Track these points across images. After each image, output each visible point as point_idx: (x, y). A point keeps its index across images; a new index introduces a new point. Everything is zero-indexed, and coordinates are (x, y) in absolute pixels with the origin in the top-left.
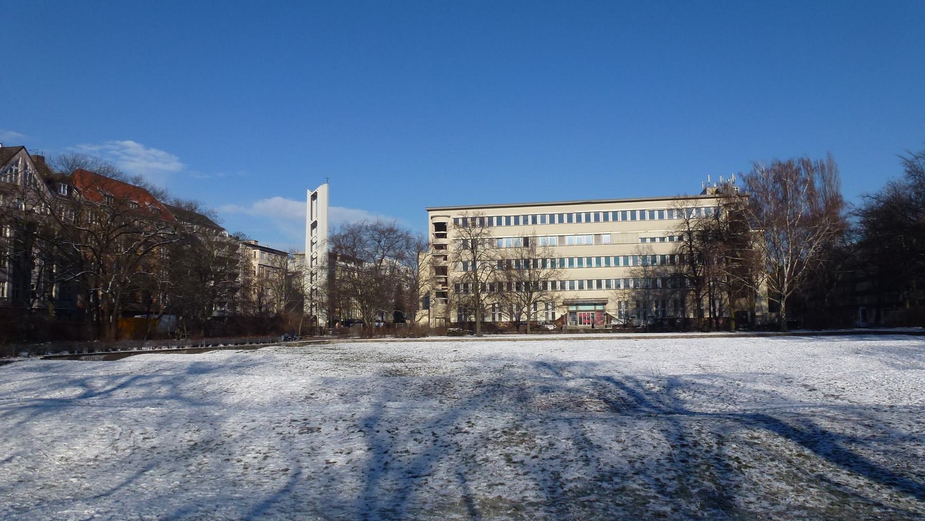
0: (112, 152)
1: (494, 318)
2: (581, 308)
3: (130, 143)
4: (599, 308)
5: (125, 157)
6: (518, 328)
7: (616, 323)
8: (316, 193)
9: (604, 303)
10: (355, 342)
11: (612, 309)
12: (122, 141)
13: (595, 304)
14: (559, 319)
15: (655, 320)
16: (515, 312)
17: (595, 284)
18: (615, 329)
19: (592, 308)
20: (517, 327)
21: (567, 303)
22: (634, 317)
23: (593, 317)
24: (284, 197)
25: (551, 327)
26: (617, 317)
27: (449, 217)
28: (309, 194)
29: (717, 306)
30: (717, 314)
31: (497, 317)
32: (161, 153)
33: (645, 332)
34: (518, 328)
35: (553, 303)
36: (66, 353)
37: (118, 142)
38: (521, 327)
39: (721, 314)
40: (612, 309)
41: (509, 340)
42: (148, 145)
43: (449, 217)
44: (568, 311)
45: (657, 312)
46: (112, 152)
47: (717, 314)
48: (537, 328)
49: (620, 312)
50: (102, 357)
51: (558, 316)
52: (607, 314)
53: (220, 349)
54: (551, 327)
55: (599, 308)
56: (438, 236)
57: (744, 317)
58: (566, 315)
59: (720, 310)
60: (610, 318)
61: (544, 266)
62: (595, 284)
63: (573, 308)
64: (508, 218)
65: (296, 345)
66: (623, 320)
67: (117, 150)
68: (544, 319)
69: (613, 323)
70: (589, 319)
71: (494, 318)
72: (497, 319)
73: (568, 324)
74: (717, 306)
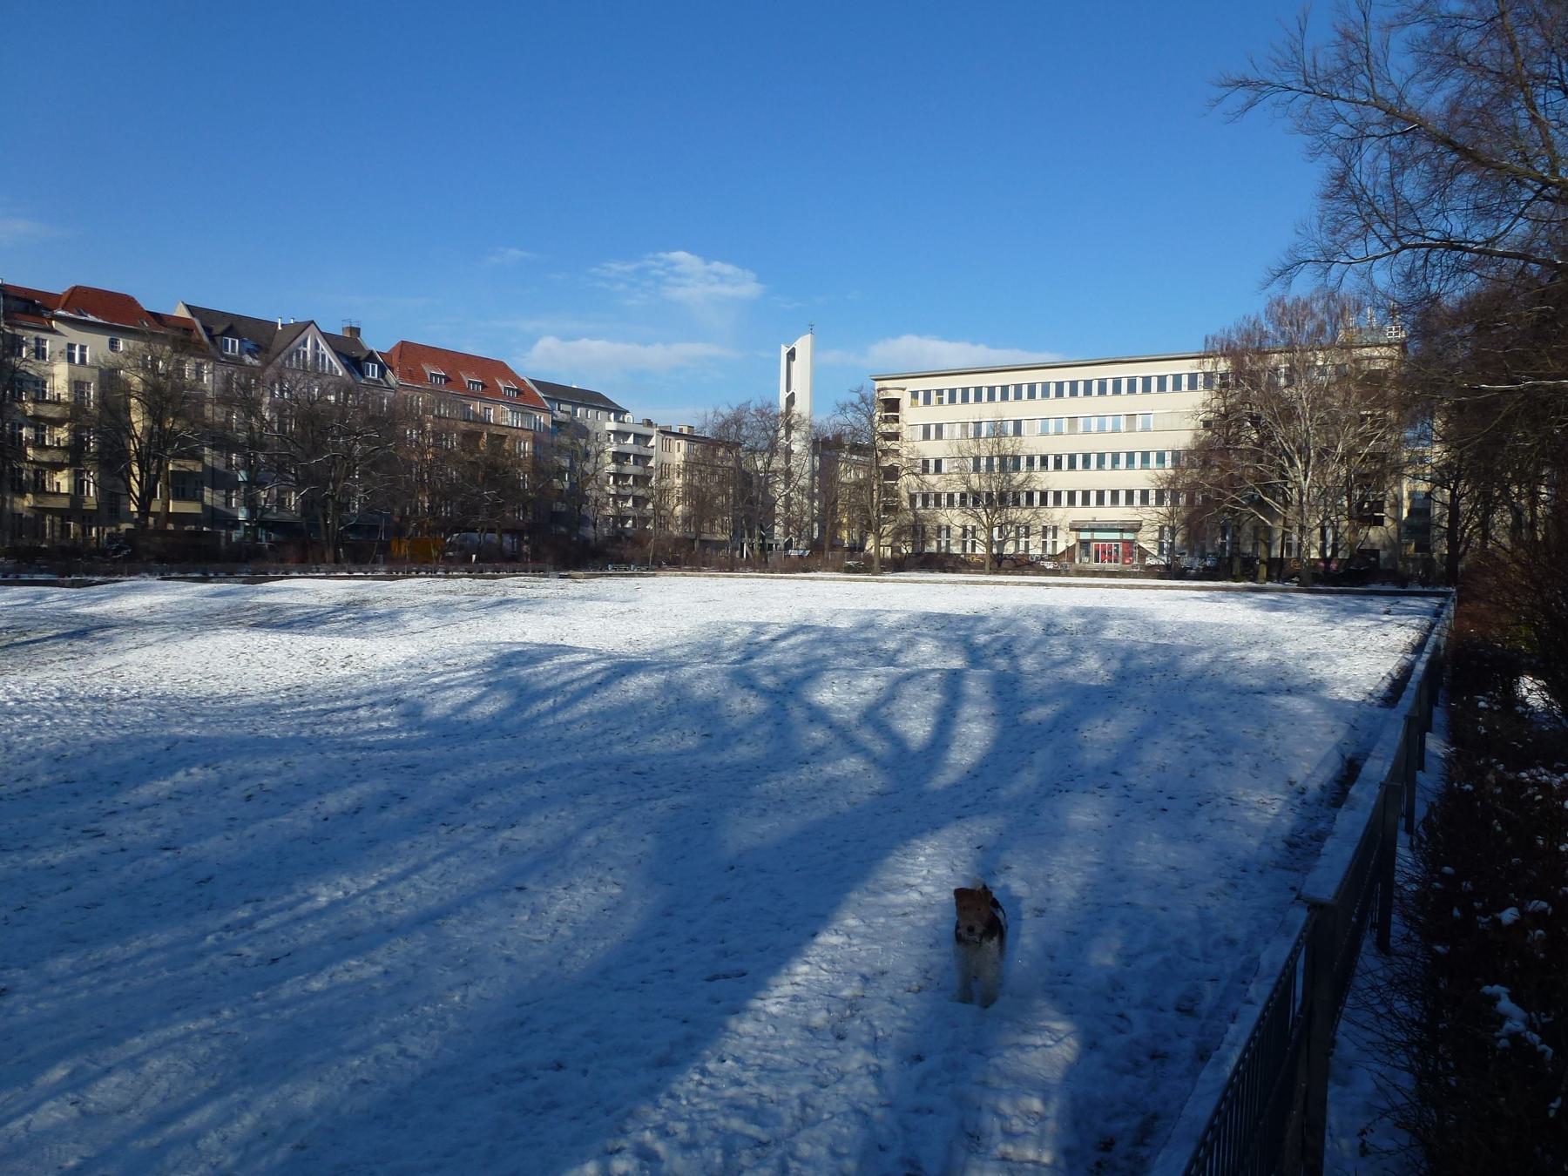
0: (653, 272)
1: (964, 548)
2: (1098, 536)
3: (680, 255)
4: (1127, 536)
5: (672, 279)
6: (999, 565)
7: (1153, 562)
8: (794, 349)
9: (1135, 528)
10: (685, 575)
11: (1147, 540)
12: (667, 251)
13: (1122, 531)
14: (1063, 553)
15: (1220, 559)
16: (997, 539)
17: (1122, 496)
18: (1151, 572)
19: (1116, 536)
20: (1000, 564)
21: (1075, 528)
22: (1184, 554)
23: (1117, 551)
24: (920, 334)
25: (1049, 565)
26: (1156, 553)
27: (904, 389)
28: (784, 351)
29: (1330, 538)
30: (1329, 553)
31: (1022, 546)
32: (728, 269)
33: (1161, 577)
34: (999, 565)
35: (1027, 528)
36: (424, 573)
37: (662, 255)
38: (1005, 564)
39: (1335, 553)
40: (1147, 540)
41: (929, 582)
42: (707, 254)
43: (904, 389)
44: (1078, 540)
45: (1223, 546)
46: (653, 272)
47: (1329, 553)
48: (1022, 565)
49: (1161, 545)
50: (241, 580)
51: (1061, 548)
52: (1139, 547)
53: (439, 577)
54: (1049, 565)
55: (1127, 536)
56: (886, 420)
57: (1373, 559)
58: (1074, 545)
59: (1334, 547)
60: (1144, 554)
61: (1017, 468)
62: (1122, 496)
63: (1085, 536)
64: (991, 390)
65: (580, 577)
66: (1165, 558)
67: (663, 269)
68: (1039, 552)
69: (1149, 561)
70: (1110, 554)
71: (964, 548)
72: (969, 551)
73: (1077, 561)
74: (1330, 538)
